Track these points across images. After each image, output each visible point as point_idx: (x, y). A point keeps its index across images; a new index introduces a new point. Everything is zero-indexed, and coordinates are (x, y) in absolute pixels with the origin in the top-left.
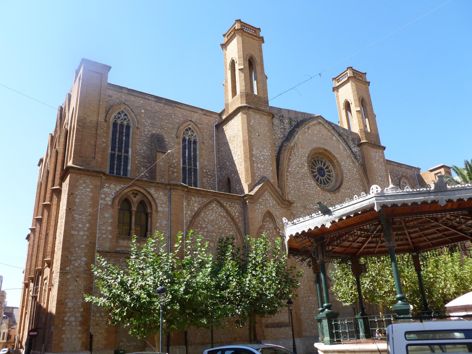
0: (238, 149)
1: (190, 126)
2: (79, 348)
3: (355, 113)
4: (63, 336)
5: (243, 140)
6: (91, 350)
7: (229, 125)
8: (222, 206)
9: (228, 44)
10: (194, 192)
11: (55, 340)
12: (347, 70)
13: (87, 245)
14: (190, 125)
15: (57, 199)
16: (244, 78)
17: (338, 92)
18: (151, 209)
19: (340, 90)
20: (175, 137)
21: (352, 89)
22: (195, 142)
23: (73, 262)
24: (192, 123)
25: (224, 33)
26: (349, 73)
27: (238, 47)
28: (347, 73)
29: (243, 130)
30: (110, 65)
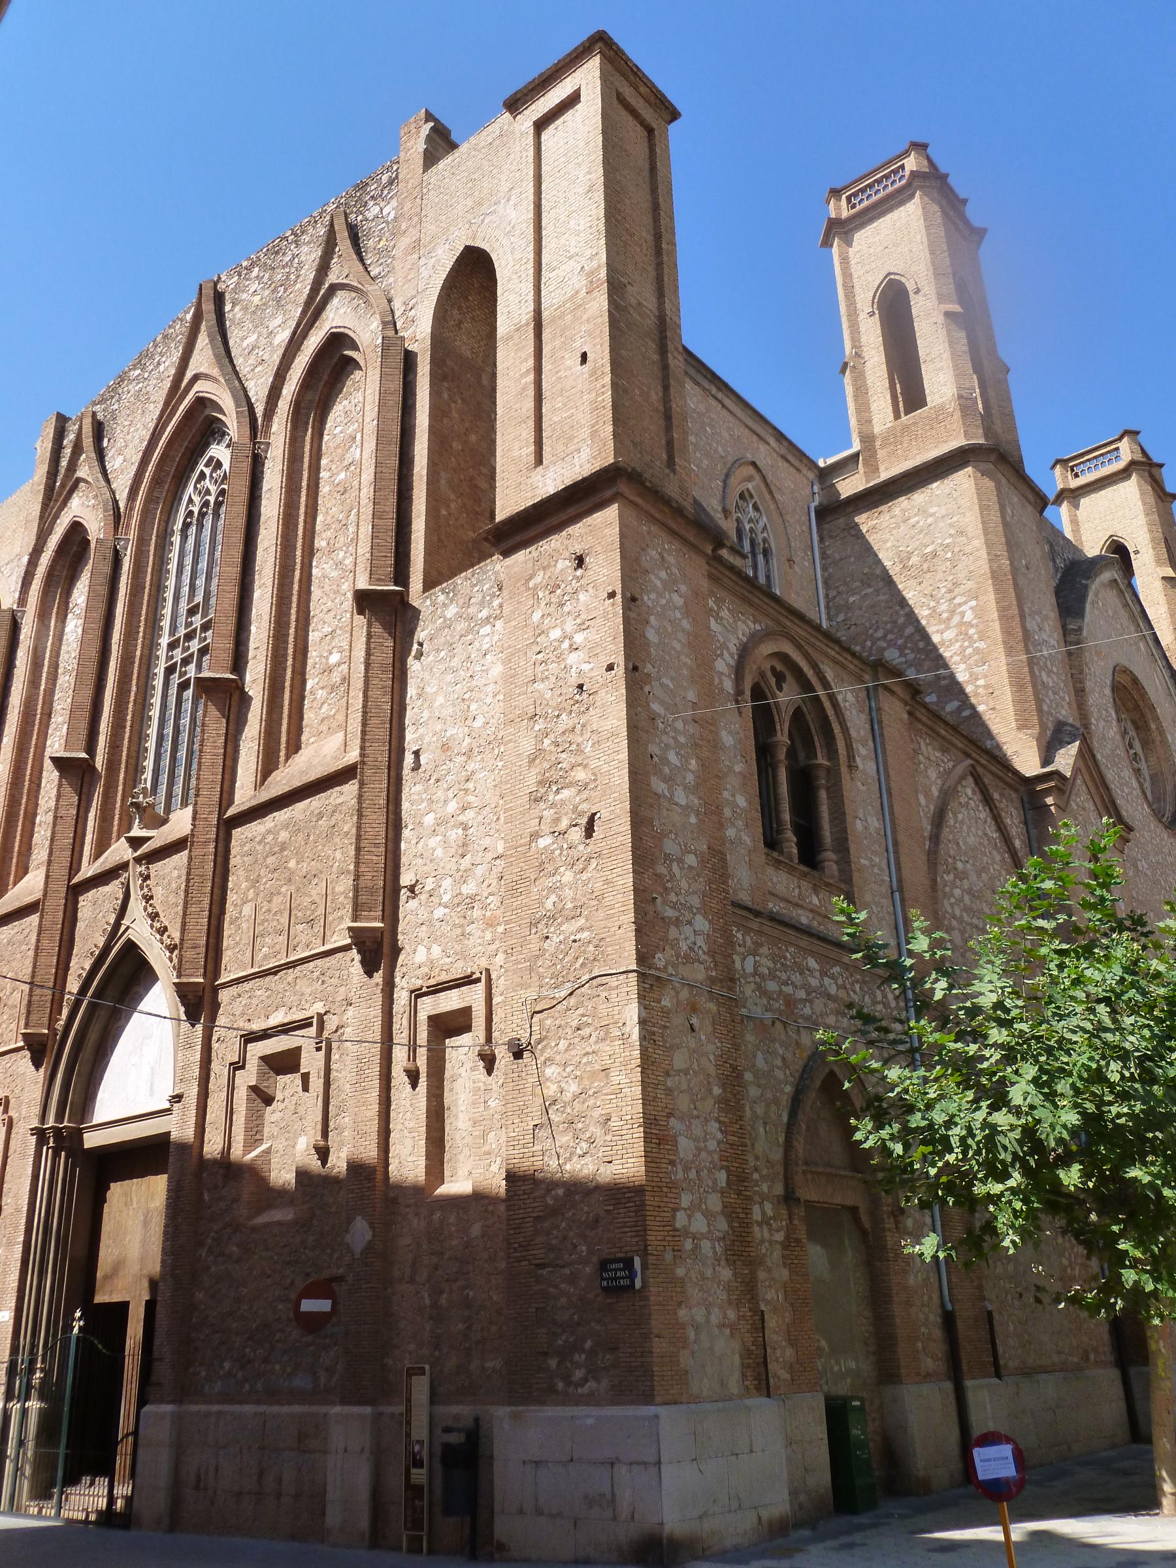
0: (958, 600)
1: (750, 486)
2: (734, 1386)
3: (1159, 585)
4: (682, 1313)
5: (993, 572)
6: (998, 1375)
7: (897, 511)
8: (987, 800)
9: (862, 225)
10: (924, 719)
11: (658, 1336)
12: (1120, 439)
13: (703, 862)
14: (750, 479)
15: (390, 643)
16: (966, 348)
17: (1077, 507)
18: (832, 753)
19: (1084, 502)
20: (720, 509)
21: (1144, 504)
22: (766, 553)
23: (673, 932)
24: (757, 477)
25: (839, 186)
26: (1126, 452)
27: (928, 235)
28: (1117, 449)
29: (986, 532)
30: (680, 107)
